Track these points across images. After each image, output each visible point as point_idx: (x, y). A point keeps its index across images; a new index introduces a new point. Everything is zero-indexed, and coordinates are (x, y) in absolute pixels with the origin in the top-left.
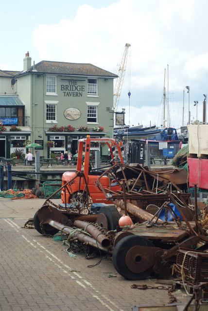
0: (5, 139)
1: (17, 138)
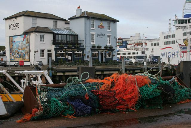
0: (72, 52)
1: (63, 52)
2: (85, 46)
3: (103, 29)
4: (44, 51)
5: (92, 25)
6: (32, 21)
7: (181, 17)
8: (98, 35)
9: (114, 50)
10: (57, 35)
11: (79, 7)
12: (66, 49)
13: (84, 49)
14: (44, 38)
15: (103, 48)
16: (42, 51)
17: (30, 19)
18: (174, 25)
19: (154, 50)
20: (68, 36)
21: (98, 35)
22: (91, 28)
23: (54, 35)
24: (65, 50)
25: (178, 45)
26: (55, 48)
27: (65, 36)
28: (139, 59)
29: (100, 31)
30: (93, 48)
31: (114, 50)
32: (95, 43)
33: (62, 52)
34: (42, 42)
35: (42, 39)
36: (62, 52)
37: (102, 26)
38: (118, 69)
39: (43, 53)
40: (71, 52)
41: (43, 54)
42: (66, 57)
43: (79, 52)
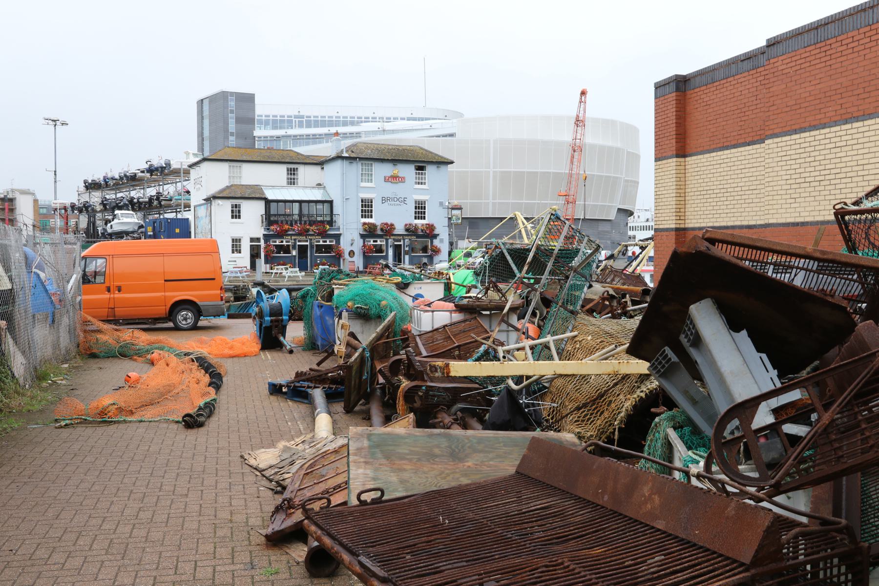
0: (308, 243)
1: (330, 242)
2: (341, 227)
5: (369, 178)
6: (230, 172)
8: (384, 200)
9: (438, 235)
10: (272, 204)
12: (291, 235)
13: (341, 234)
15: (400, 229)
16: (236, 239)
17: (225, 165)
18: (574, 151)
19: (64, 127)
20: (303, 204)
21: (384, 200)
22: (364, 184)
23: (268, 202)
25: (394, 288)
27: (297, 204)
29: (391, 189)
30: (370, 232)
31: (438, 235)
32: (377, 219)
35: (236, 214)
37: (398, 177)
39: (240, 245)
40: (307, 241)
41: (240, 247)
43: (328, 243)
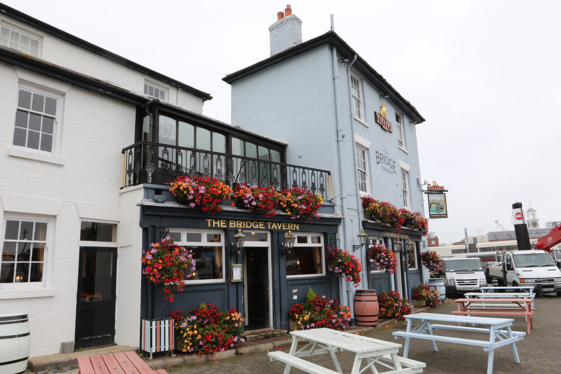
0: (267, 244)
1: (190, 238)
2: (338, 202)
3: (388, 132)
4: (42, 228)
7: (101, 366)
11: (288, 10)
14: (57, 128)
24: (222, 224)
26: (144, 208)
28: (459, 272)
33: (198, 238)
34: (25, 151)
36: (204, 243)
38: (482, 306)
42: (229, 274)
